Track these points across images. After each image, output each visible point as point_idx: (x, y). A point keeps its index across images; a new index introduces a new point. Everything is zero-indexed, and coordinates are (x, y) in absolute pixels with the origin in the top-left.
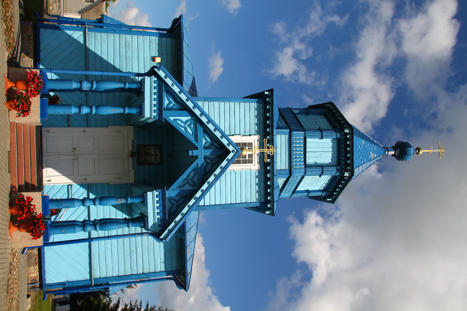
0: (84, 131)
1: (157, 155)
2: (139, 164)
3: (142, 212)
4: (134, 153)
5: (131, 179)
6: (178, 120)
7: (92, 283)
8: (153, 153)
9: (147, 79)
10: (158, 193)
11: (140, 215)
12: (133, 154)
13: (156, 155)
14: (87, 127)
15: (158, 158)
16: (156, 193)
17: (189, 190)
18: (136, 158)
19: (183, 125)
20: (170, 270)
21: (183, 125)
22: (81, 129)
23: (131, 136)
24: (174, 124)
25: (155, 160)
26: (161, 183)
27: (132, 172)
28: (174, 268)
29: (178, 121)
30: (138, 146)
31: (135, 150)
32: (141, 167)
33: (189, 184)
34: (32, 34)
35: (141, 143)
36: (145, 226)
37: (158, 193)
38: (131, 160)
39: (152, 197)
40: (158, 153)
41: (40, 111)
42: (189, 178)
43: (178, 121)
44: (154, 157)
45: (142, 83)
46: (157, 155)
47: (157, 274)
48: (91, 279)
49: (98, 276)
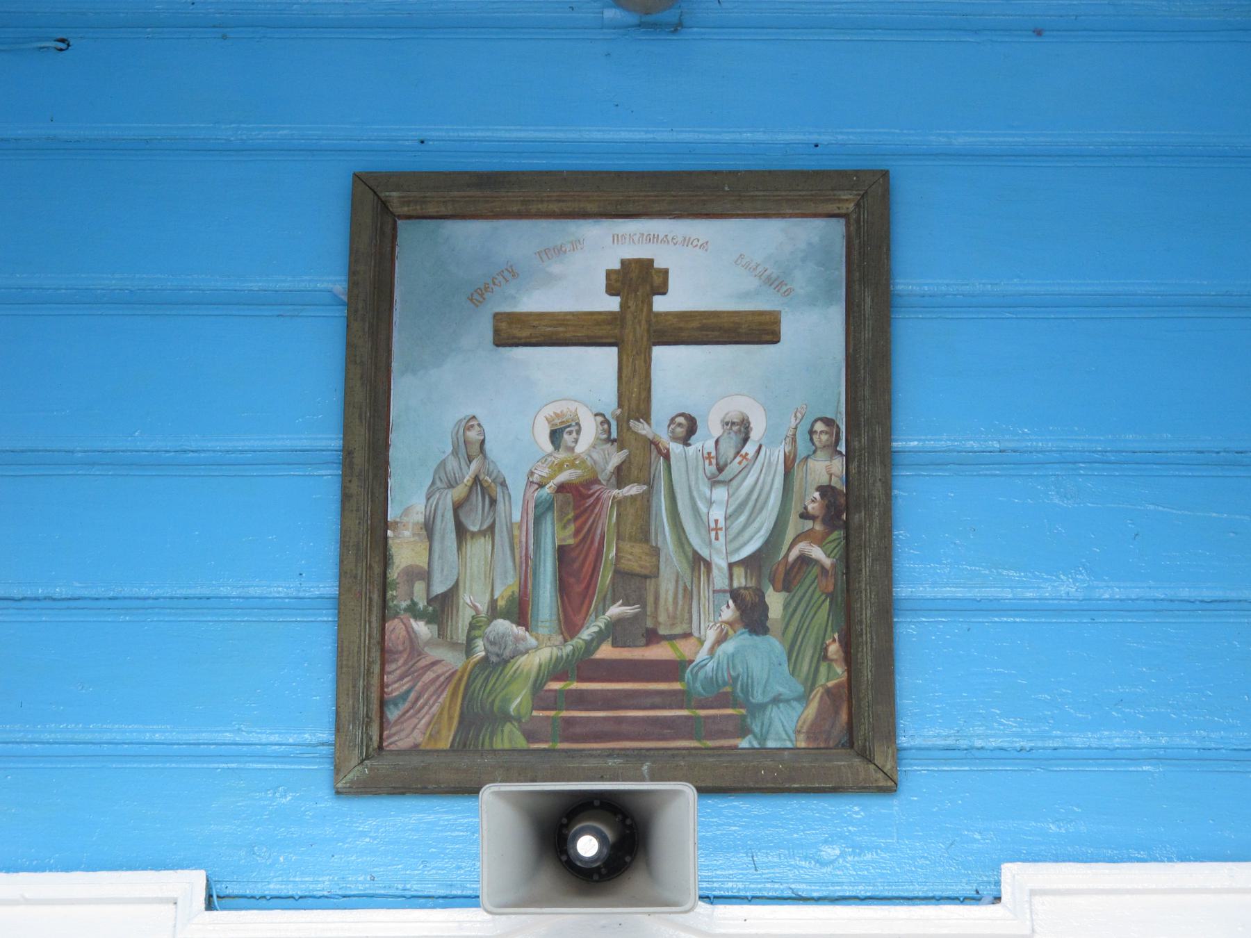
1: (637, 280)
2: (855, 745)
13: (636, 321)
15: (703, 263)
25: (757, 330)
30: (377, 760)
40: (578, 266)
46: (637, 280)
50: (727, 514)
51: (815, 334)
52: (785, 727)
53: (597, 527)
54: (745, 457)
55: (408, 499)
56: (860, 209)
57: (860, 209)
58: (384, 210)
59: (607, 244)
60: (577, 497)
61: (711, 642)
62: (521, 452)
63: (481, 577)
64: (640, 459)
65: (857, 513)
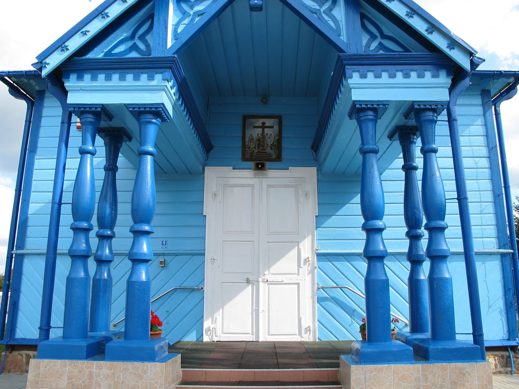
0: (213, 260)
1: (264, 123)
2: (279, 158)
3: (387, 133)
4: (257, 165)
5: (310, 173)
6: (175, 31)
7: (509, 254)
8: (260, 130)
9: (72, 99)
10: (356, 75)
11: (397, 136)
12: (260, 167)
14: (204, 254)
15: (268, 122)
16: (354, 79)
17: (347, 10)
18: (268, 164)
19: (186, 21)
20: (481, 109)
21: (186, 21)
22: (208, 266)
23: (227, 171)
24: (184, 39)
25: (272, 127)
26: (331, 65)
27: (296, 172)
28: (478, 101)
29: (179, 31)
30: (245, 159)
31: (252, 164)
32: (283, 156)
33: (330, 9)
34: (24, 352)
35: (239, 154)
36: (434, 108)
37: (356, 75)
38: (272, 173)
39: (364, 87)
41: (136, 363)
42: (318, 8)
43: (179, 31)
44: (266, 130)
45: (82, 110)
46: (264, 123)
47: (489, 132)
48: (503, 255)
49: (494, 241)
50: (270, 141)
51: (276, 128)
52: (274, 157)
53: (261, 141)
54: (306, 260)
55: (247, 140)
56: (279, 118)
57: (279, 118)
58: (245, 118)
59: (261, 121)
60: (259, 140)
61: (268, 150)
62: (255, 136)
63: (252, 145)
64: (264, 137)
65: (279, 141)
